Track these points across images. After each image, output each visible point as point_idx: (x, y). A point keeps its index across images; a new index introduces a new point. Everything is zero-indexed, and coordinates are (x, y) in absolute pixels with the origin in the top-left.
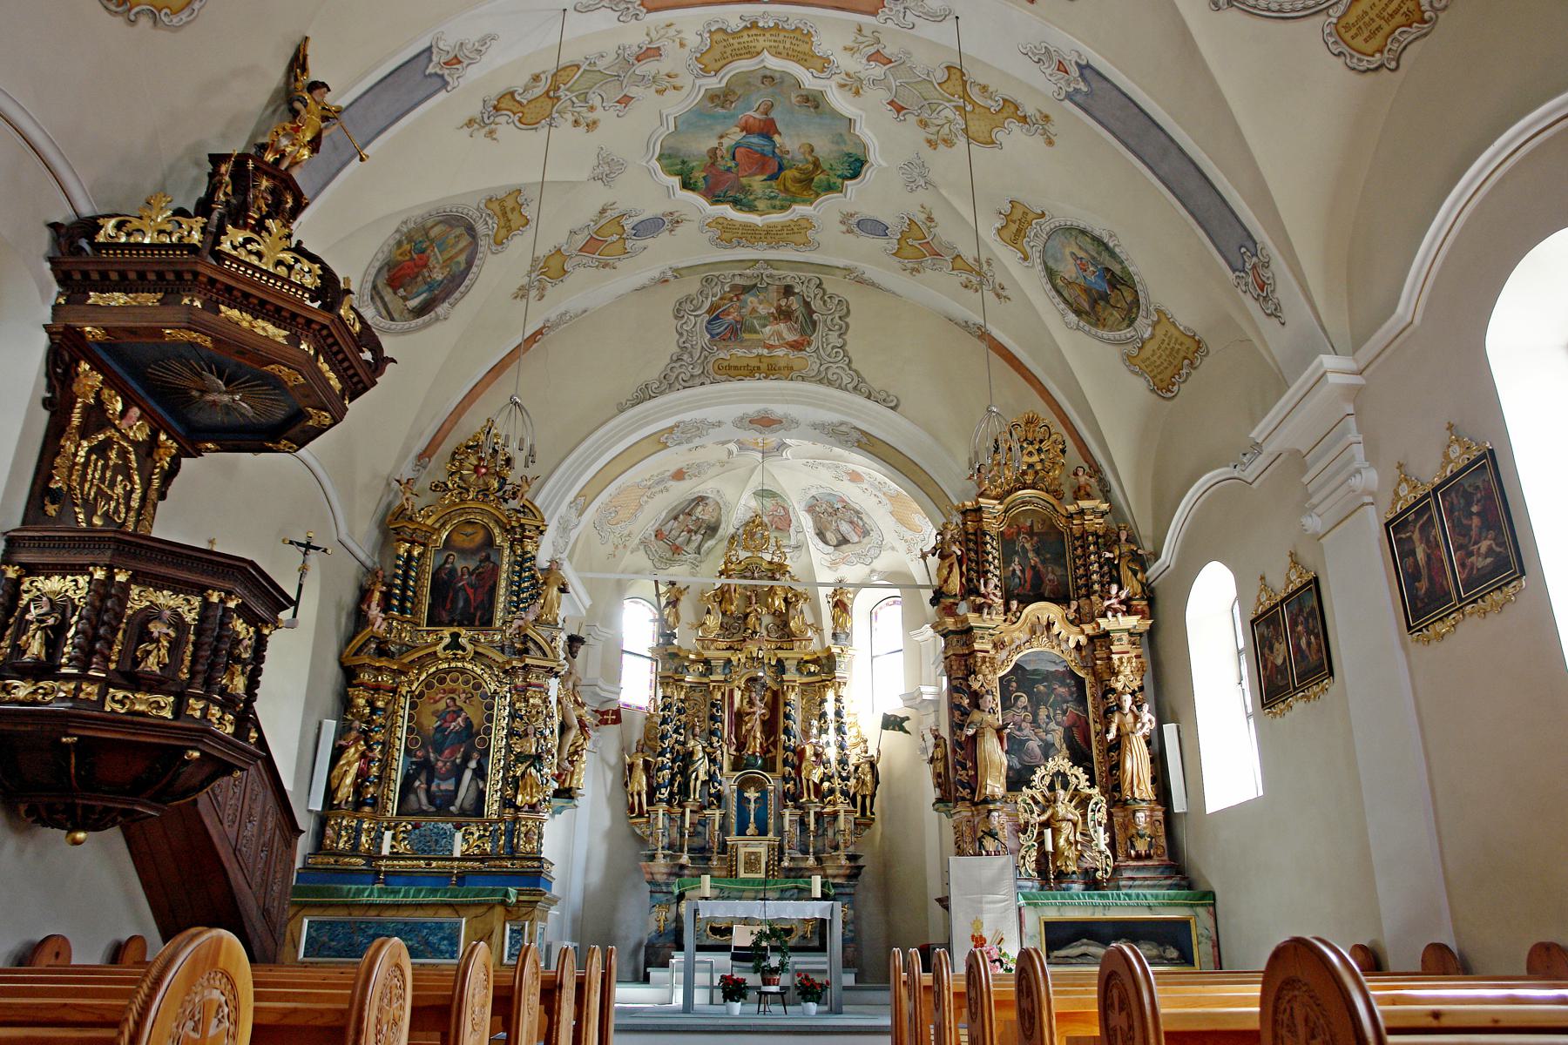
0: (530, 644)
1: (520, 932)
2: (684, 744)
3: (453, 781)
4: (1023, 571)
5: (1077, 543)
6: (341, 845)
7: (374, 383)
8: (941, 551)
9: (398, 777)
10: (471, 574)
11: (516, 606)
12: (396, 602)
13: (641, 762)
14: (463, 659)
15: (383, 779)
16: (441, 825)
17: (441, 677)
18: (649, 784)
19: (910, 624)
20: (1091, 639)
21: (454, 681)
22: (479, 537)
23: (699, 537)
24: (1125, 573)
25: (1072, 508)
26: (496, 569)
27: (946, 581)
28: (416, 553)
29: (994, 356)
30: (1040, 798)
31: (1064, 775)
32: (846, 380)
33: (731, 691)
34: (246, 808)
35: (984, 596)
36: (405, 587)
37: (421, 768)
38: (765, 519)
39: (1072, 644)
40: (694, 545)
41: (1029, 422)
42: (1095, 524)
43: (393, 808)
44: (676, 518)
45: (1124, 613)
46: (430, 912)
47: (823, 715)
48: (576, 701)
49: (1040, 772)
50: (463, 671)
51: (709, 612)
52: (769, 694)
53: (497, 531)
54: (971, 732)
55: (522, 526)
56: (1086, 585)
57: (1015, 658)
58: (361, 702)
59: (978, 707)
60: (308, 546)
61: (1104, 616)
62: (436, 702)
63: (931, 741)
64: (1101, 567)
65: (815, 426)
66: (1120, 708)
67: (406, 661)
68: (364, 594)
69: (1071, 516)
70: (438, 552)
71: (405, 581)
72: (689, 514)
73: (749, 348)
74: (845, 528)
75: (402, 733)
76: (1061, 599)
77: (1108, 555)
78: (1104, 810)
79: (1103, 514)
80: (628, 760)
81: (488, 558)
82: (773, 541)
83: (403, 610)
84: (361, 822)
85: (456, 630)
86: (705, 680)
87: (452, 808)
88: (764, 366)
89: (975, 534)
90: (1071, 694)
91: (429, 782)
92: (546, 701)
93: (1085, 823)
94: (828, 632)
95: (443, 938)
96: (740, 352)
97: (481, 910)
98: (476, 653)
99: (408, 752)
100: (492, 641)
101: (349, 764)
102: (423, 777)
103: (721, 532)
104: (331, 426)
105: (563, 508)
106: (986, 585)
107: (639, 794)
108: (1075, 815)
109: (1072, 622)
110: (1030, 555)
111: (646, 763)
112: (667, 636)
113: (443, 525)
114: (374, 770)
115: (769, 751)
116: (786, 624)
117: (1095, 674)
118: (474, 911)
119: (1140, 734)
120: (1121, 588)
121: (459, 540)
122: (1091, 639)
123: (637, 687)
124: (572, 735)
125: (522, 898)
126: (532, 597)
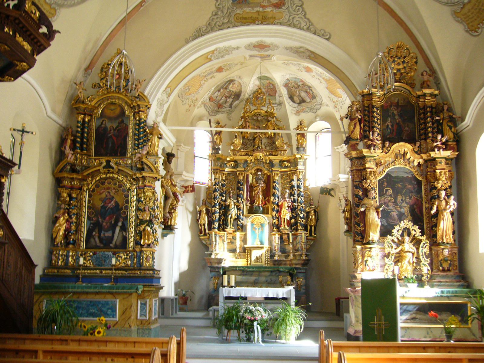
0: (145, 166)
1: (145, 304)
2: (225, 201)
3: (111, 232)
4: (392, 126)
5: (421, 111)
6: (60, 263)
7: (50, 45)
8: (350, 116)
9: (84, 230)
10: (115, 130)
11: (138, 146)
12: (78, 145)
13: (204, 210)
14: (113, 173)
15: (78, 231)
16: (106, 253)
17: (102, 182)
18: (209, 221)
19: (334, 144)
20: (426, 161)
21: (109, 183)
22: (118, 111)
23: (231, 100)
24: (446, 128)
25: (419, 93)
26: (126, 128)
27: (352, 132)
28: (87, 120)
29: (380, 8)
30: (396, 240)
31: (409, 229)
32: (303, 24)
33: (248, 176)
34: (6, 260)
35: (372, 141)
36: (82, 137)
37: (95, 226)
38: (264, 90)
39: (416, 164)
40: (229, 104)
41: (398, 47)
42: (429, 101)
43: (83, 245)
44: (219, 91)
45: (444, 149)
46: (103, 296)
47: (292, 187)
48: (172, 184)
49: (397, 228)
50: (113, 179)
51: (236, 137)
52: (266, 177)
53: (126, 108)
54: (363, 209)
55: (138, 105)
56: (424, 123)
57: (387, 170)
58: (65, 195)
59: (367, 196)
60: (23, 131)
61: (434, 150)
62: (101, 194)
63: (343, 201)
64: (433, 124)
65: (287, 48)
66: (439, 197)
67: (85, 174)
68: (62, 141)
69: (418, 97)
70: (98, 119)
71: (82, 134)
72: (226, 89)
73: (252, 8)
74: (303, 94)
75: (85, 210)
76: (411, 140)
77: (437, 118)
78: (428, 247)
79: (436, 96)
80: (198, 209)
81: (122, 122)
82: (267, 101)
83: (82, 149)
84: (68, 252)
85: (108, 158)
86: (234, 170)
87: (111, 245)
88: (260, 17)
89: (368, 107)
90: (414, 188)
91: (100, 233)
92: (154, 193)
93: (418, 252)
94: (294, 147)
95: (109, 309)
96: (247, 10)
97: (126, 296)
98: (119, 170)
99: (89, 218)
100: (126, 164)
101: (60, 225)
102: (97, 230)
103: (242, 97)
104: (28, 69)
105: (159, 95)
106: (373, 135)
107: (204, 225)
108: (414, 250)
109: (416, 153)
110: (397, 117)
111: (207, 210)
112: (215, 150)
113: (100, 105)
114: (73, 228)
115: (265, 204)
116: (274, 143)
117: (426, 179)
118: (122, 296)
119: (448, 211)
120: (443, 136)
121: (108, 112)
122: (426, 161)
123: (202, 174)
124: (170, 202)
125: (145, 289)
126: (145, 141)
